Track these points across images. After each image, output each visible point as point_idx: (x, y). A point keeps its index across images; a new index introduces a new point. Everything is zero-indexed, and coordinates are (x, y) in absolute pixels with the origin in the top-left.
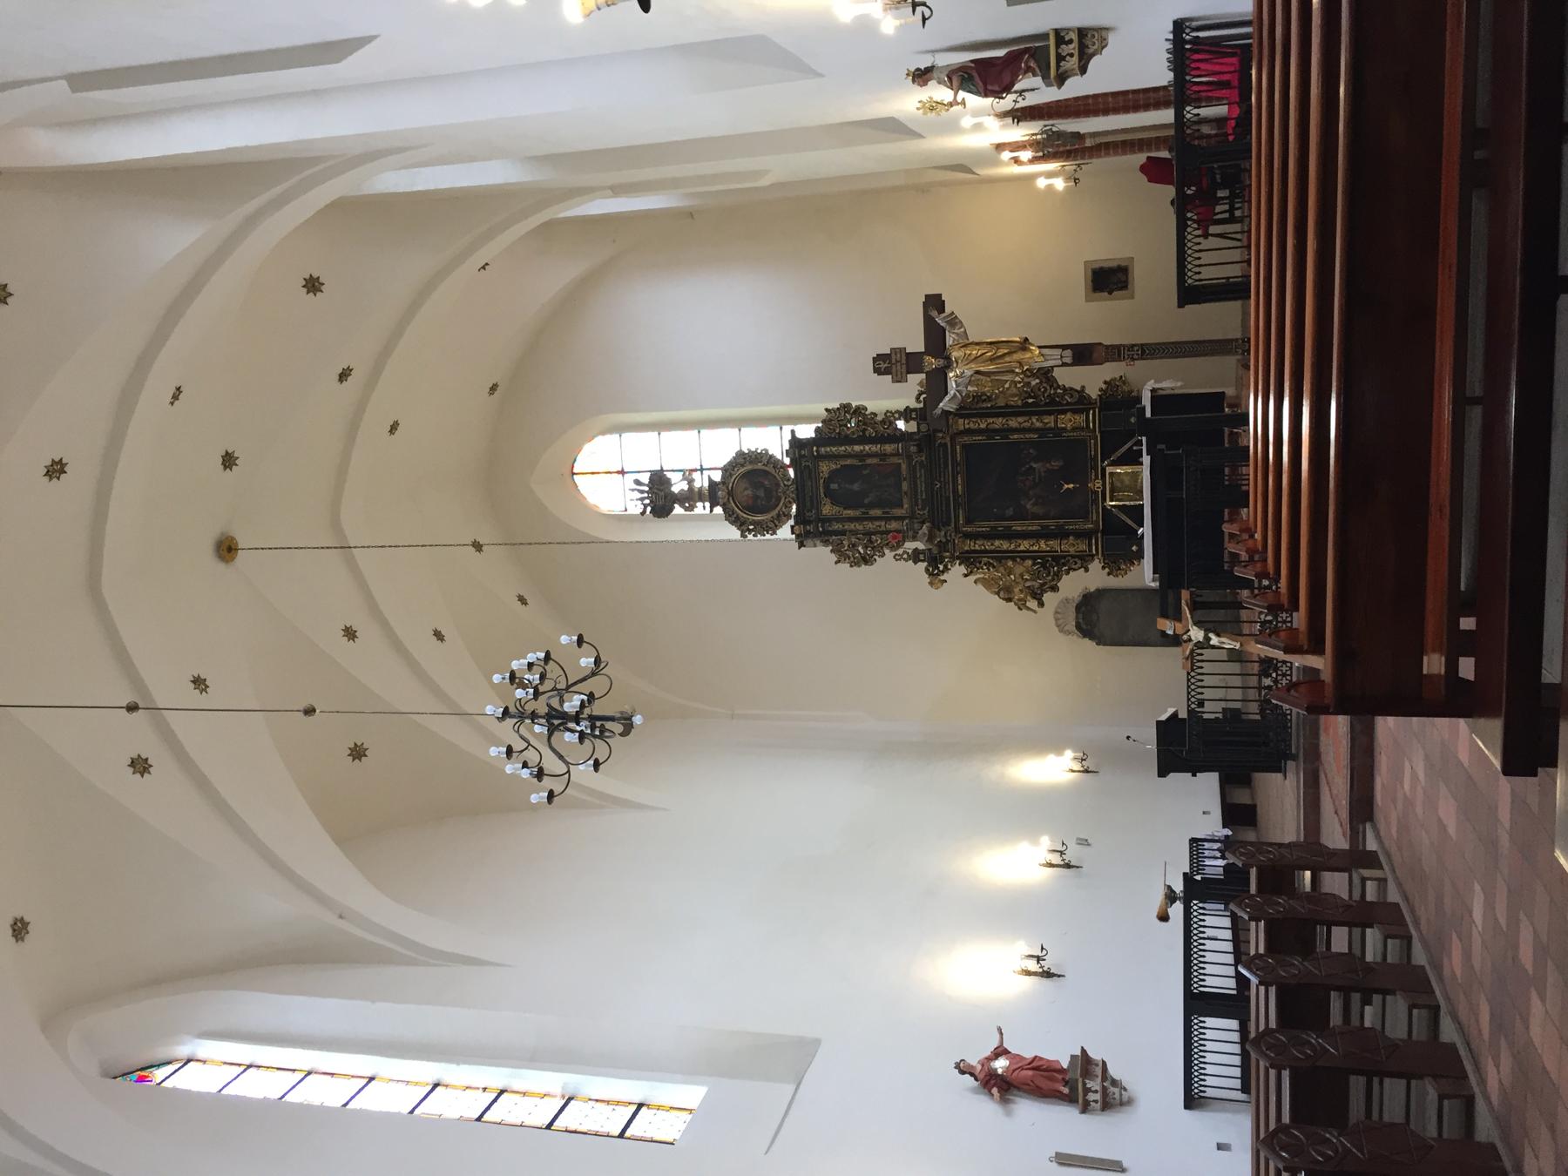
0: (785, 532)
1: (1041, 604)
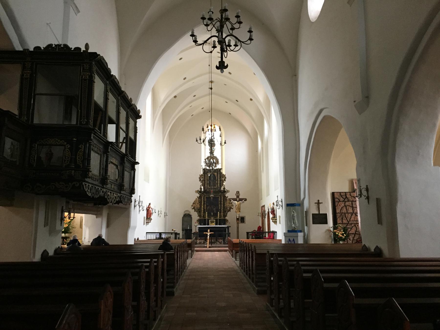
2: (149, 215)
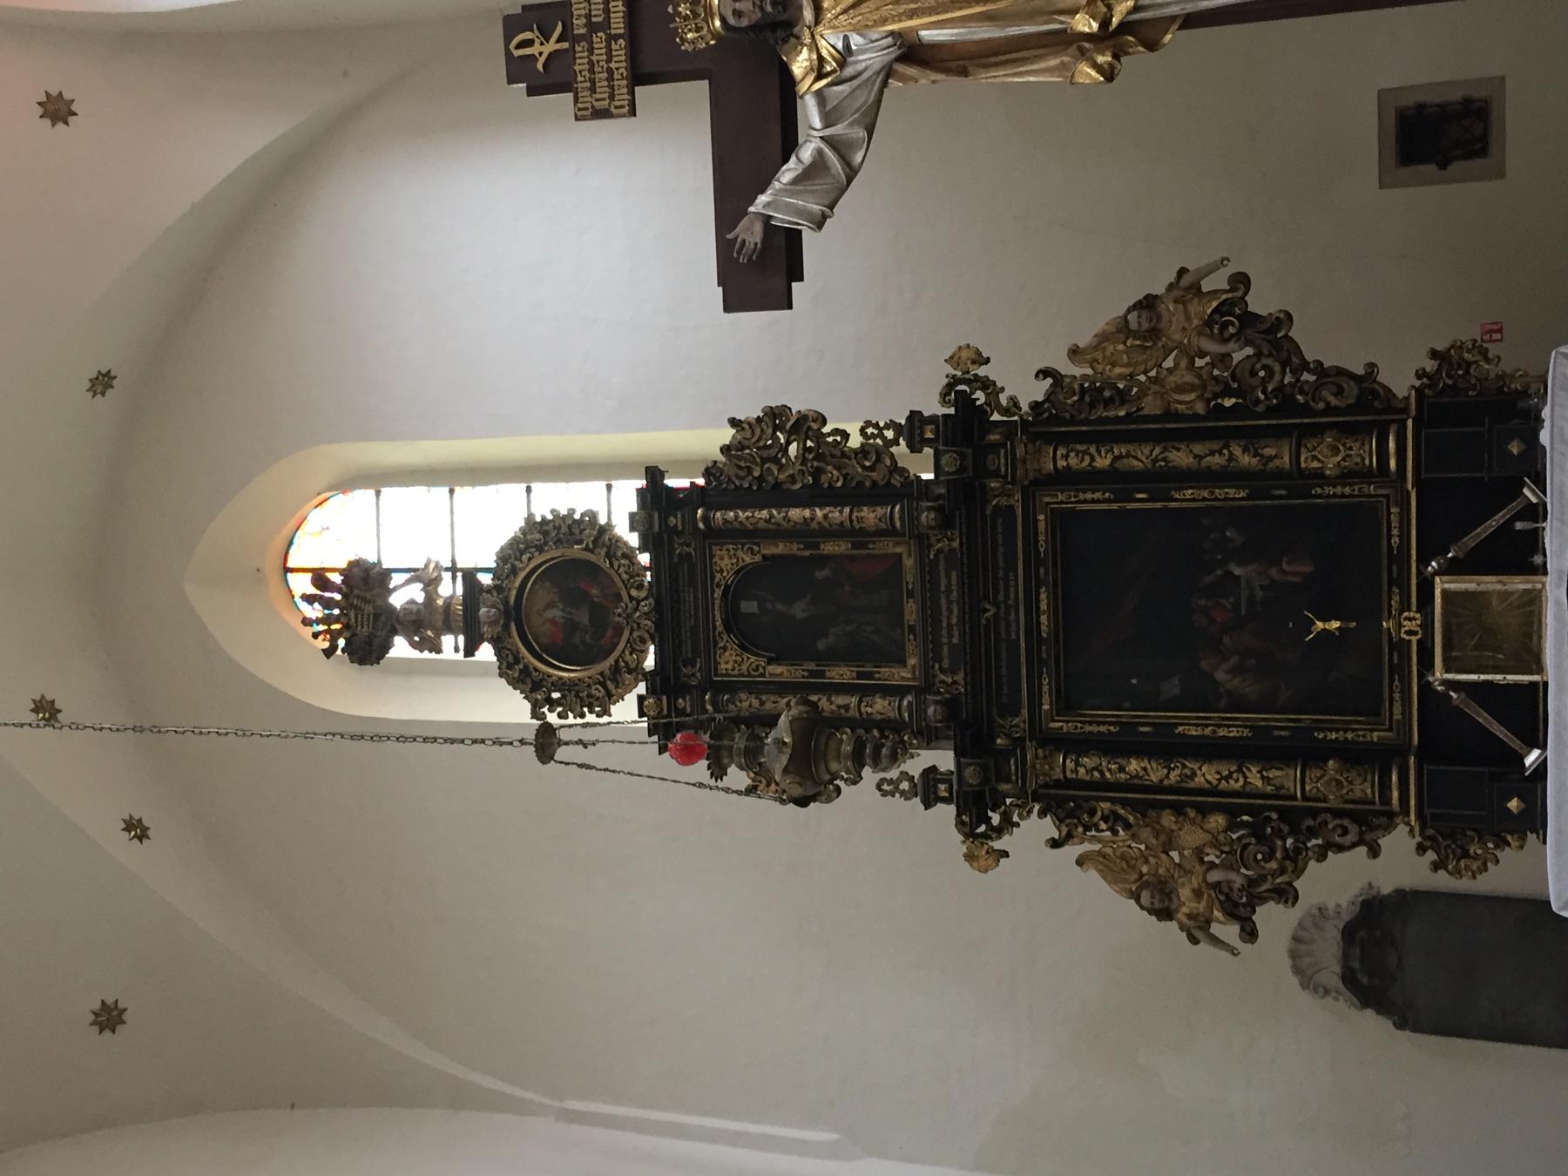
0: (625, 710)
1: (1250, 934)
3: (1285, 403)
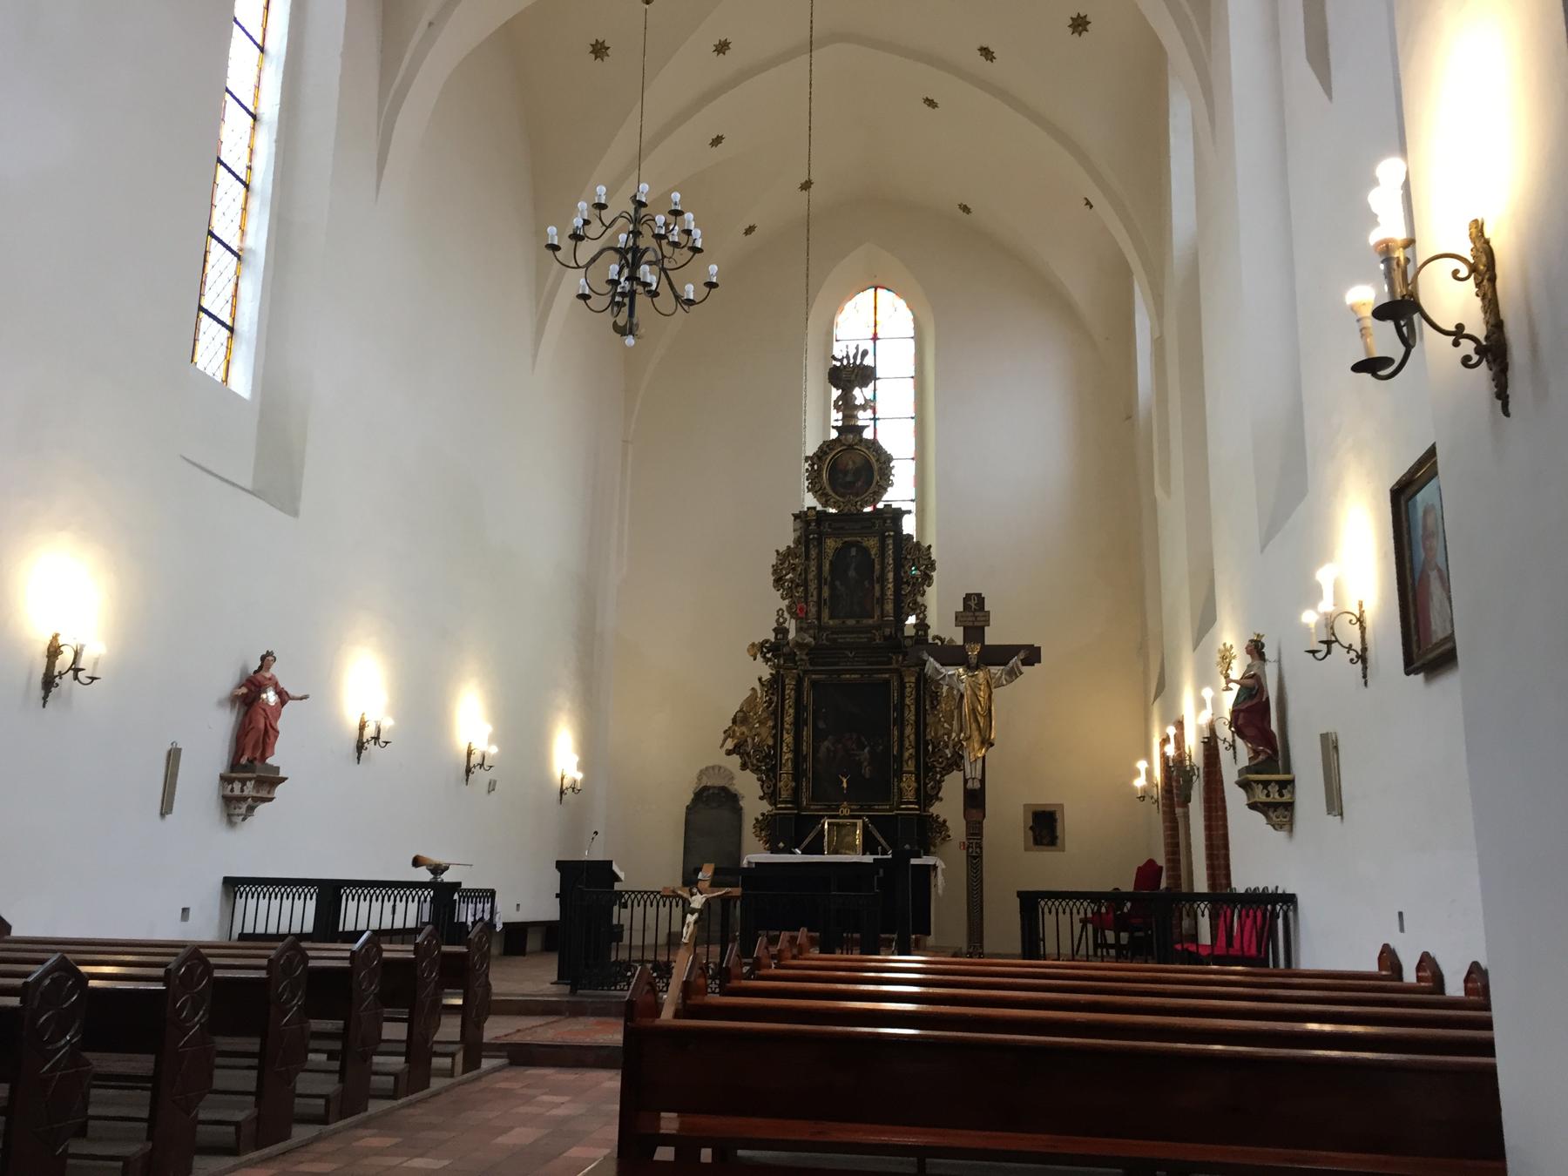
0: (810, 501)
1: (729, 753)
2: (250, 741)
3: (929, 769)
